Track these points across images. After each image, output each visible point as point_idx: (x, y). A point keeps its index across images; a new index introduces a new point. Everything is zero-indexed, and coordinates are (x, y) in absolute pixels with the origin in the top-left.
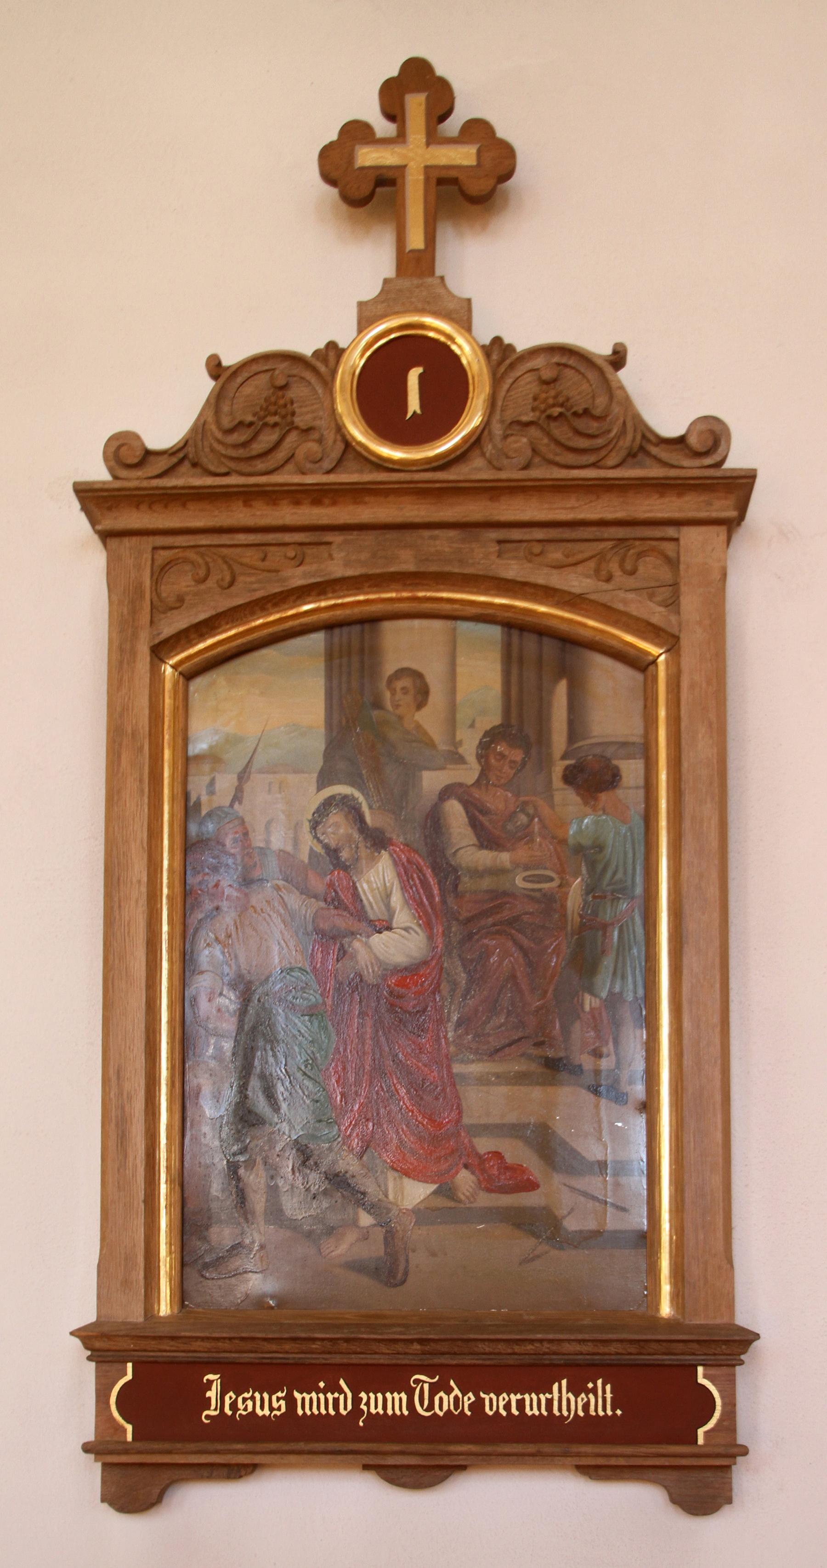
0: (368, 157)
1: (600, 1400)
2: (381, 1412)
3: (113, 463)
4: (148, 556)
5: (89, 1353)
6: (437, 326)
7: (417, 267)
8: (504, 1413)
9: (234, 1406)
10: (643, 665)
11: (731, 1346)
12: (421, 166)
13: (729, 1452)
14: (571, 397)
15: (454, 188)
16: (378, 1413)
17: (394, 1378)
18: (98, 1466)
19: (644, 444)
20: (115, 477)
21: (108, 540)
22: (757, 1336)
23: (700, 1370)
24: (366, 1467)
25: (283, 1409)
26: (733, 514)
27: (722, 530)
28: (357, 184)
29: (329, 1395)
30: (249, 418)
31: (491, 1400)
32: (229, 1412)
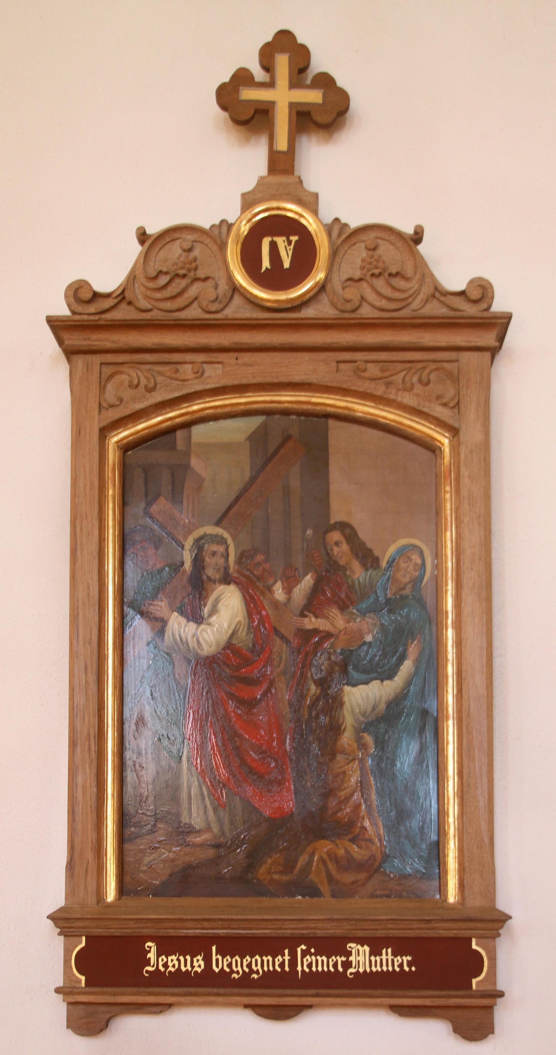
1: (389, 961)
3: (72, 300)
4: (97, 368)
5: (59, 930)
6: (292, 209)
9: (166, 965)
10: (432, 448)
12: (286, 100)
14: (390, 251)
18: (66, 1003)
20: (74, 313)
21: (71, 356)
22: (510, 918)
23: (474, 941)
24: (246, 1006)
25: (203, 967)
26: (494, 343)
27: (488, 355)
28: (241, 108)
29: (318, 957)
32: (162, 969)
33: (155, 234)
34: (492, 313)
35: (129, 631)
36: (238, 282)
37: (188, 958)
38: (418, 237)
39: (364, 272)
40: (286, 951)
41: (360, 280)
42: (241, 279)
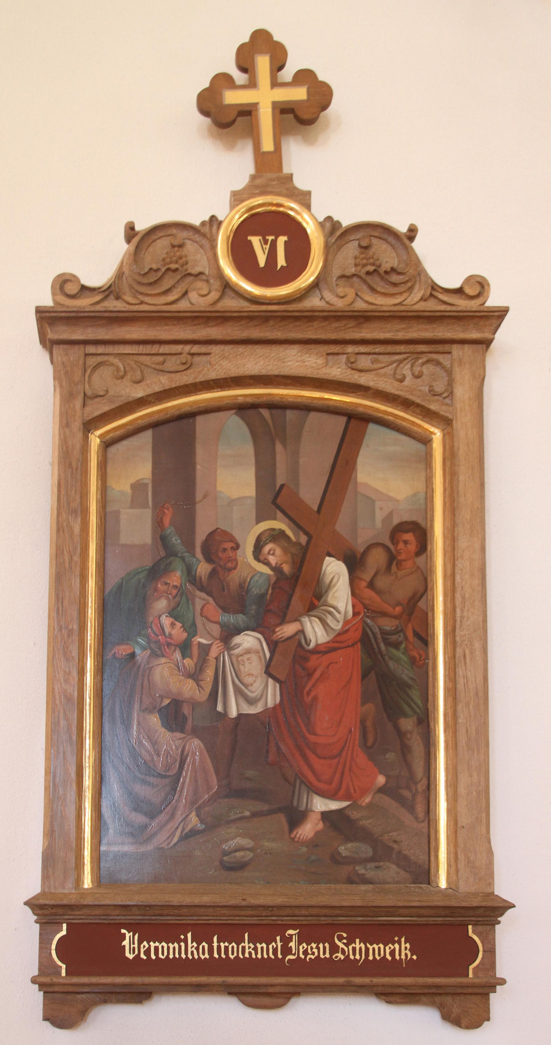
0: (232, 98)
5: (35, 917)
6: (292, 207)
7: (269, 170)
11: (491, 911)
12: (265, 102)
13: (490, 985)
14: (380, 251)
15: (291, 116)
17: (171, 933)
18: (42, 993)
19: (434, 293)
23: (470, 927)
24: (230, 994)
28: (223, 115)
30: (154, 266)
31: (233, 947)
32: (303, 957)
33: (142, 230)
35: (468, 623)
37: (171, 956)
38: (412, 232)
39: (359, 268)
40: (278, 938)
41: (354, 275)
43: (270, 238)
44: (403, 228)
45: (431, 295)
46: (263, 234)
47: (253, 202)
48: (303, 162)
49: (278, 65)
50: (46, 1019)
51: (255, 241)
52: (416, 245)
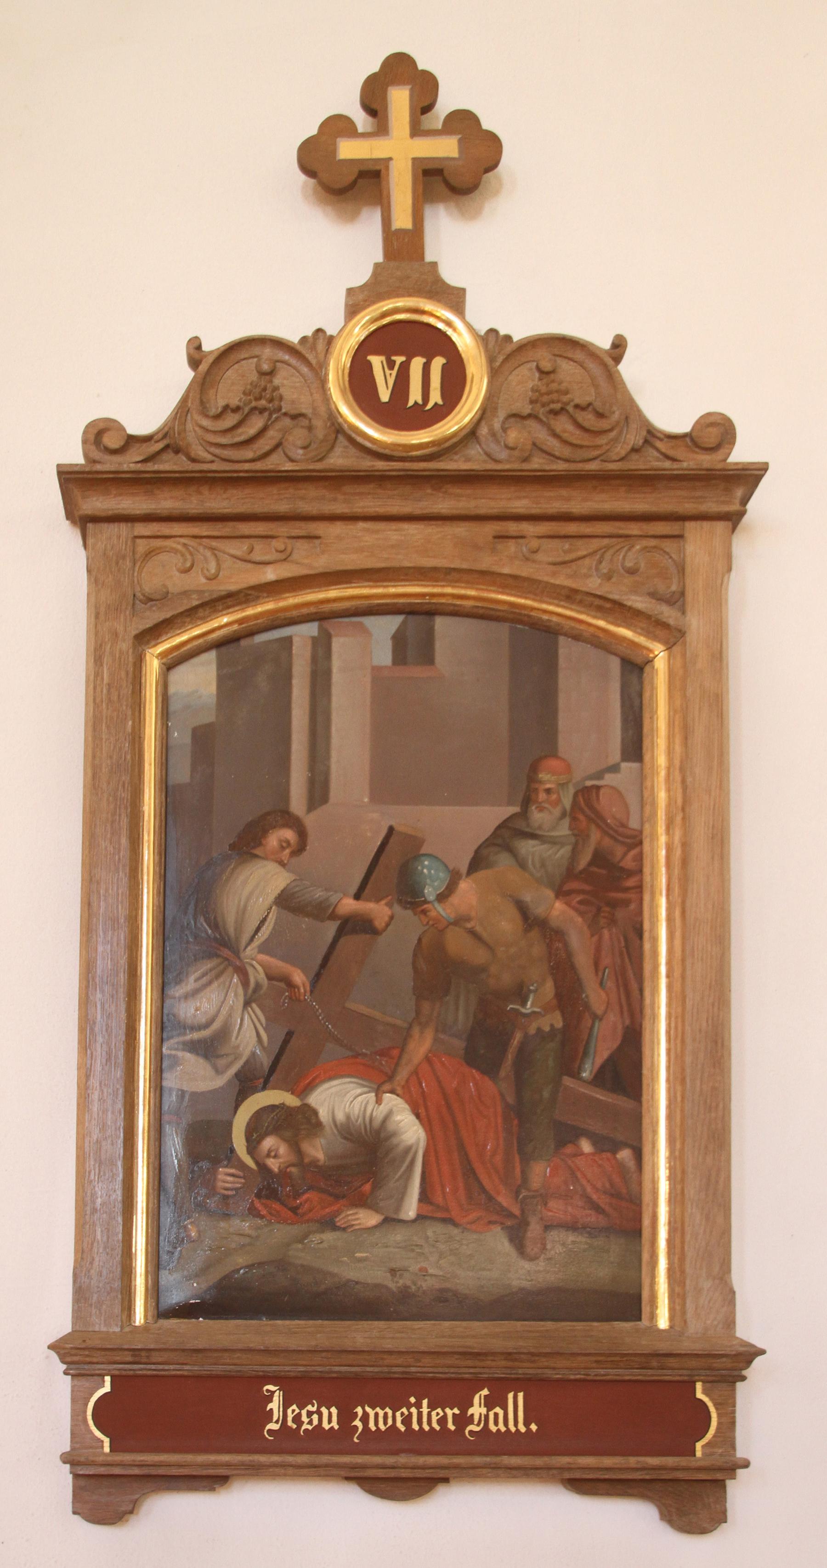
0: (349, 150)
2: (503, 1429)
5: (64, 1367)
6: (438, 315)
7: (404, 251)
8: (402, 1428)
9: (297, 1419)
11: (731, 1364)
12: (403, 156)
14: (569, 381)
15: (438, 178)
16: (332, 1428)
23: (699, 1386)
24: (348, 1479)
26: (735, 507)
28: (339, 179)
30: (234, 402)
34: (730, 463)
36: (346, 421)
38: (619, 346)
41: (530, 416)
42: (349, 414)
43: (399, 359)
44: (604, 343)
45: (646, 441)
46: (388, 353)
47: (383, 306)
48: (454, 243)
49: (424, 105)
50: (75, 1513)
51: (377, 361)
52: (623, 368)
